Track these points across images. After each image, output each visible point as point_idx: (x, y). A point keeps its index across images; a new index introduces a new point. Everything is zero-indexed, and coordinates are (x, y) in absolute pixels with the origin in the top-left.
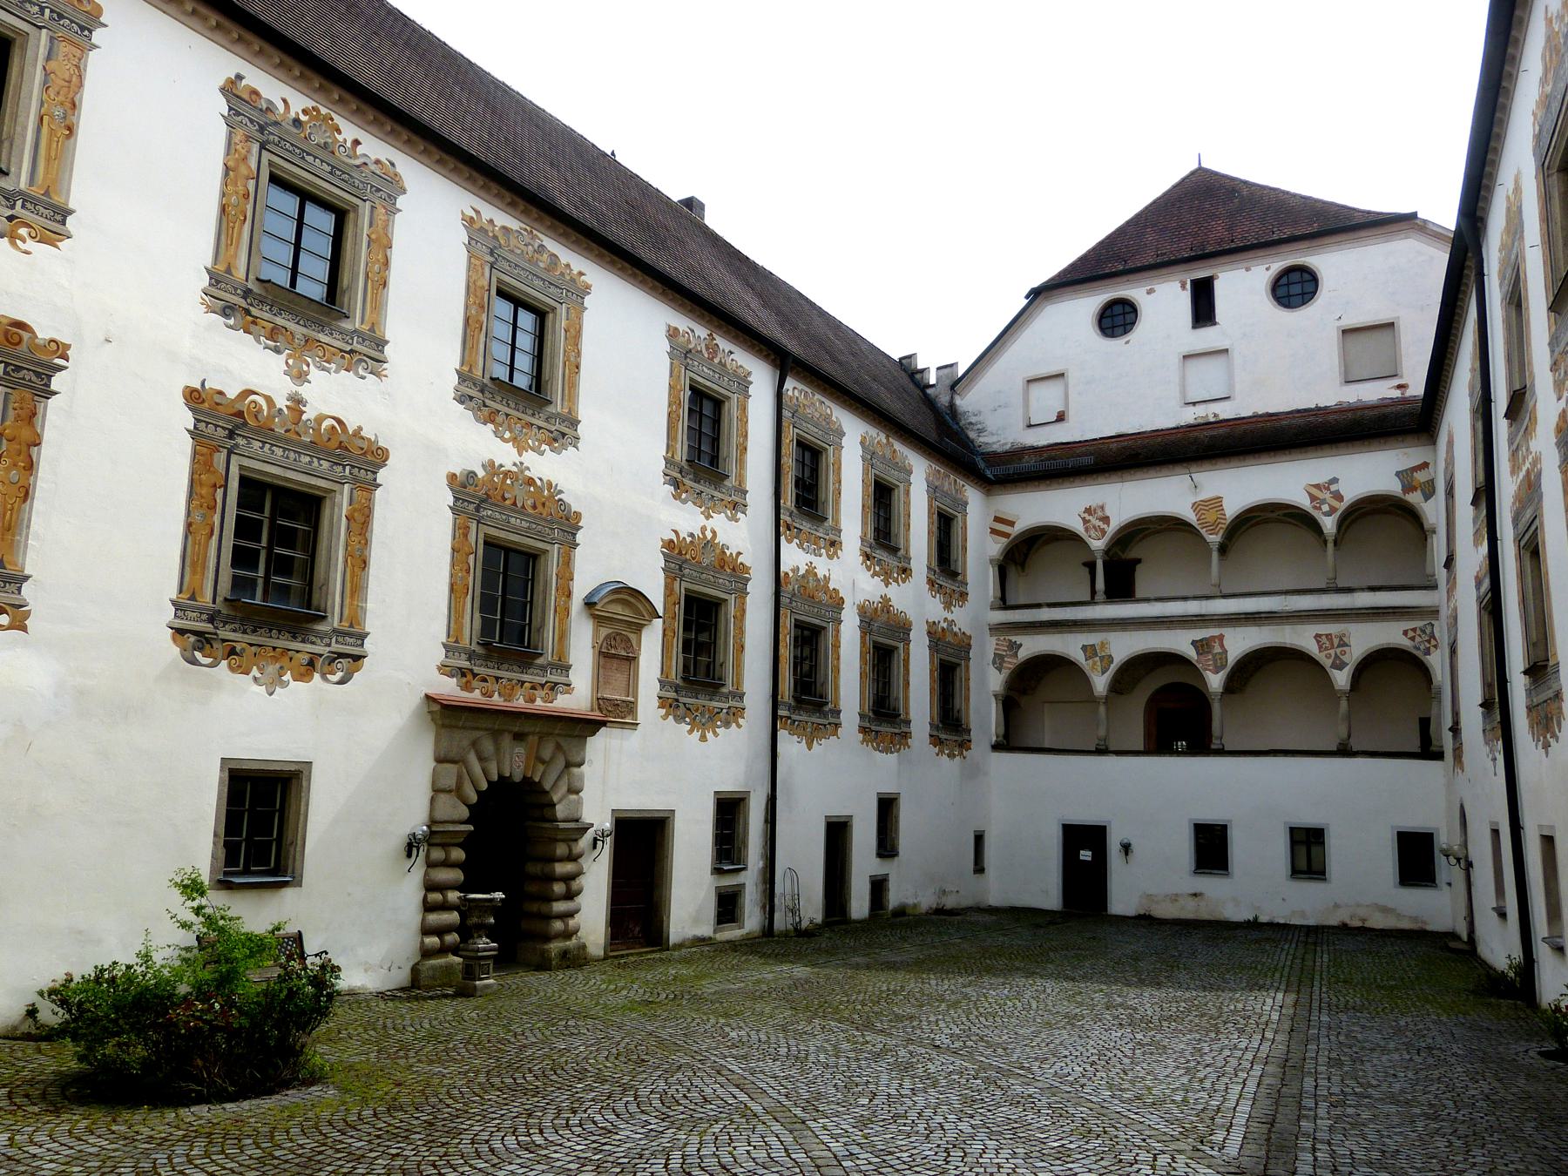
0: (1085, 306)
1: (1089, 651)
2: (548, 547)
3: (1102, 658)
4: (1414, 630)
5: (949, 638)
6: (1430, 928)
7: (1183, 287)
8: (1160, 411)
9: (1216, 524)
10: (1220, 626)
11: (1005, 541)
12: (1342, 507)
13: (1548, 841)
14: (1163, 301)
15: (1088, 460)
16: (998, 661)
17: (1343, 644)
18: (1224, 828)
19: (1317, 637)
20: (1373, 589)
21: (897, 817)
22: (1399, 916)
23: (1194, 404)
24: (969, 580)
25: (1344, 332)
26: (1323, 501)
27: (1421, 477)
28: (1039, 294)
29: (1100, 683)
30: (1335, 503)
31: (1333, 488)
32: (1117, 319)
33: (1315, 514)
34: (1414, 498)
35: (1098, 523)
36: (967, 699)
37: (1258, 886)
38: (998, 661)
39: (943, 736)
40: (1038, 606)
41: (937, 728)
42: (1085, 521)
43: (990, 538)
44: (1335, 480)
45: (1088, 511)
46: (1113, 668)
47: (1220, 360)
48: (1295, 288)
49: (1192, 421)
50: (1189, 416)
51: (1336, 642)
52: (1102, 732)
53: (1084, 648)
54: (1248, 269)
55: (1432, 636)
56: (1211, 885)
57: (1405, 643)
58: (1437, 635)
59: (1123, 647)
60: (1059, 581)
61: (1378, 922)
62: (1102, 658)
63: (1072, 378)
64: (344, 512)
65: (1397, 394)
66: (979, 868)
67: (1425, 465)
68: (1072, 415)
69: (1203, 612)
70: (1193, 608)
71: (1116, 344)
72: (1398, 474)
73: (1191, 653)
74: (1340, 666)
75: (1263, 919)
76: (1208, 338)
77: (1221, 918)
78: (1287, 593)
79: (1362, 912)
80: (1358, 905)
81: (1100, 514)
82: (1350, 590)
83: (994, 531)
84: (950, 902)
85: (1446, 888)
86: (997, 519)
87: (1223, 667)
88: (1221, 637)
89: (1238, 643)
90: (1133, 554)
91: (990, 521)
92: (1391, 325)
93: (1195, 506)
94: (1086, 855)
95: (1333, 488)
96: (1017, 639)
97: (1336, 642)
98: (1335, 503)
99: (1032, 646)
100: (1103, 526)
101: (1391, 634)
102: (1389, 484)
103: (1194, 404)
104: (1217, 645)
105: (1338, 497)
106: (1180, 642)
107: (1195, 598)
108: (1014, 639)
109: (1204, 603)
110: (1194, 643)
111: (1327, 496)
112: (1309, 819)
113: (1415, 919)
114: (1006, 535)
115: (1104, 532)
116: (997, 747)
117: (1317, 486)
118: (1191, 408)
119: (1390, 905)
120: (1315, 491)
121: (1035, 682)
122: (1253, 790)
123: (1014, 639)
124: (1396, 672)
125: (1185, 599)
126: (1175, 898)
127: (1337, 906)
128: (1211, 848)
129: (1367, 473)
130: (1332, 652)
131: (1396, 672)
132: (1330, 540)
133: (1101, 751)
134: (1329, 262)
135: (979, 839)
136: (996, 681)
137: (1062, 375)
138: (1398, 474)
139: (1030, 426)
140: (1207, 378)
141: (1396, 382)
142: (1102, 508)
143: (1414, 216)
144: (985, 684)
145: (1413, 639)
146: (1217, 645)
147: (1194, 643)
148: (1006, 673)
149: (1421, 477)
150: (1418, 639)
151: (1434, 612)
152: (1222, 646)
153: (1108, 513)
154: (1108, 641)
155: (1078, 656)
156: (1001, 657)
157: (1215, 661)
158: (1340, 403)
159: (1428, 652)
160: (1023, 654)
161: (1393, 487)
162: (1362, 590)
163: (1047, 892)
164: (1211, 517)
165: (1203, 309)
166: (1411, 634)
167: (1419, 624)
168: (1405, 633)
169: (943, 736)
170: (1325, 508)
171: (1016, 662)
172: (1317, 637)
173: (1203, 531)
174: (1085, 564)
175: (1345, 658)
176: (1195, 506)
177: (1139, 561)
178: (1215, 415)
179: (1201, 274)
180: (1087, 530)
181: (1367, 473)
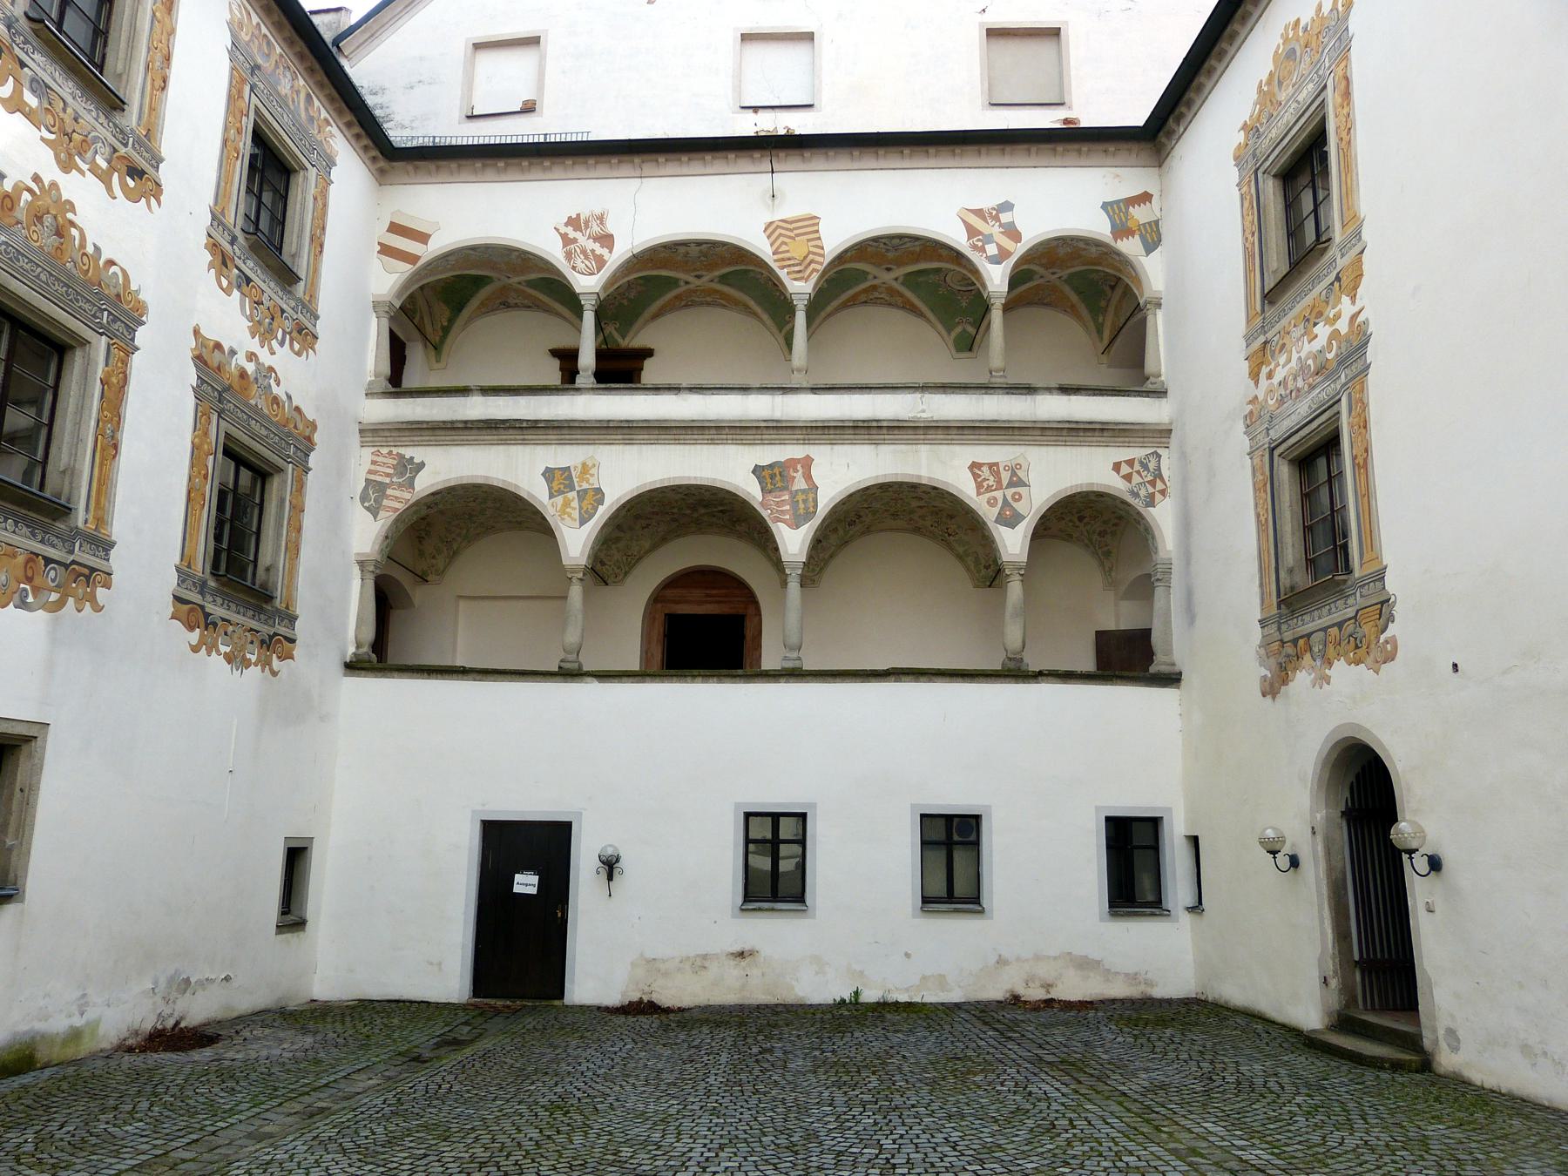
1: (558, 479)
2: (87, 333)
3: (582, 495)
4: (1130, 463)
5: (257, 400)
6: (1159, 992)
9: (806, 262)
11: (406, 269)
12: (1019, 250)
13: (1195, 841)
16: (373, 495)
17: (1017, 482)
18: (568, 825)
19: (975, 466)
20: (1065, 390)
21: (28, 804)
22: (1108, 974)
23: (756, 109)
24: (323, 307)
26: (989, 239)
27: (1140, 214)
29: (576, 542)
30: (1008, 244)
33: (974, 257)
34: (1130, 247)
36: (294, 549)
37: (863, 937)
38: (373, 495)
39: (217, 610)
40: (464, 391)
41: (202, 588)
42: (567, 240)
43: (376, 263)
44: (1007, 207)
45: (574, 222)
46: (603, 513)
47: (798, 52)
51: (1005, 477)
52: (572, 636)
53: (549, 474)
55: (1159, 475)
56: (773, 932)
57: (1114, 484)
58: (1165, 473)
59: (627, 473)
60: (508, 346)
61: (1073, 988)
62: (582, 495)
63: (551, 45)
64: (100, 374)
66: (291, 916)
67: (1145, 198)
69: (777, 415)
72: (1105, 206)
73: (751, 490)
75: (870, 996)
77: (790, 998)
79: (1044, 971)
80: (1038, 958)
81: (596, 229)
82: (1030, 390)
83: (386, 250)
84: (197, 1010)
85: (1186, 919)
86: (395, 228)
88: (807, 462)
89: (840, 473)
90: (637, 341)
91: (381, 233)
93: (771, 229)
94: (526, 883)
96: (416, 453)
97: (1005, 477)
98: (1008, 244)
100: (599, 250)
101: (1092, 469)
103: (756, 109)
104: (799, 476)
105: (1013, 233)
106: (731, 469)
107: (764, 389)
108: (408, 452)
110: (757, 470)
111: (995, 230)
113: (1133, 978)
115: (601, 262)
116: (353, 667)
117: (979, 213)
118: (750, 114)
119: (1095, 955)
121: (445, 545)
122: (852, 743)
123: (408, 452)
124: (1094, 528)
125: (745, 390)
126: (701, 963)
127: (1001, 962)
128: (775, 862)
129: (1062, 203)
130: (999, 494)
133: (569, 673)
135: (296, 856)
136: (365, 534)
139: (471, 117)
142: (601, 219)
144: (334, 540)
145: (1128, 478)
146: (799, 476)
147: (757, 470)
148: (386, 519)
149: (1140, 214)
150: (1136, 479)
151: (1162, 434)
153: (611, 228)
154: (587, 466)
155: (535, 489)
156: (381, 488)
157: (794, 504)
159: (1151, 501)
160: (426, 483)
161: (1097, 226)
162: (1049, 390)
163: (433, 958)
164: (798, 250)
167: (1137, 453)
169: (217, 610)
170: (992, 250)
171: (409, 497)
172: (975, 466)
173: (783, 274)
174: (555, 353)
176: (771, 229)
177: (648, 353)
180: (569, 256)
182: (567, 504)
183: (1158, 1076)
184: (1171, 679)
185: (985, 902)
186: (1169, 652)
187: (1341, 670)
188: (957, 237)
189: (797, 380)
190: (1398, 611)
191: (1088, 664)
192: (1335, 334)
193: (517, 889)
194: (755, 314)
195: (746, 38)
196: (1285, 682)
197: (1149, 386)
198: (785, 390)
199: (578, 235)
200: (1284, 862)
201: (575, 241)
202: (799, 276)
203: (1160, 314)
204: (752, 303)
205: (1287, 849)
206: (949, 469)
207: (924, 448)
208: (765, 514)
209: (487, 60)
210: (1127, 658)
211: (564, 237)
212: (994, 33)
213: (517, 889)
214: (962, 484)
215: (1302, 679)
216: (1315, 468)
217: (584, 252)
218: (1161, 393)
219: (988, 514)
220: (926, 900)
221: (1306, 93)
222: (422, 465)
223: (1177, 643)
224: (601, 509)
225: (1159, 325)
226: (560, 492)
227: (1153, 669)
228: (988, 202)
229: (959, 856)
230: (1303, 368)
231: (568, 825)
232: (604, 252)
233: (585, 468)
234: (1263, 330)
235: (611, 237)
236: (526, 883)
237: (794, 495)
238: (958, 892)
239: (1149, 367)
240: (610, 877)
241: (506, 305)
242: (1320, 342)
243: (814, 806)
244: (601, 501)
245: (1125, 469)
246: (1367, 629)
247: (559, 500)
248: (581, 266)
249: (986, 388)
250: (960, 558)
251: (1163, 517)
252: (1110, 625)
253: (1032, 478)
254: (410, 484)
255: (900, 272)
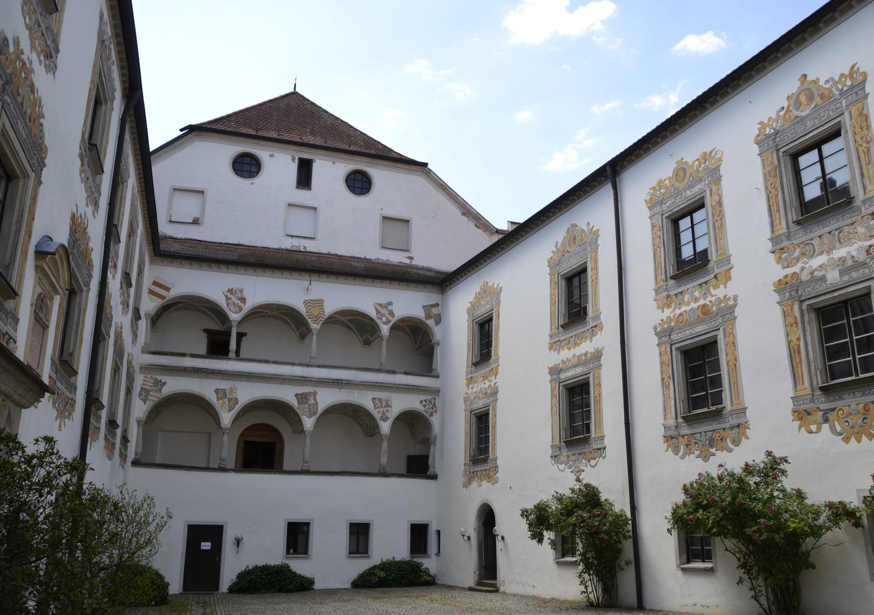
0: (226, 151)
3: (230, 400)
4: (426, 401)
7: (293, 160)
8: (270, 237)
10: (315, 386)
12: (394, 320)
13: (439, 532)
14: (279, 165)
15: (234, 256)
19: (374, 399)
20: (406, 373)
23: (292, 236)
25: (384, 217)
26: (383, 315)
28: (191, 130)
30: (390, 318)
31: (390, 308)
32: (247, 166)
34: (431, 323)
35: (237, 301)
40: (183, 355)
42: (227, 298)
44: (390, 304)
45: (230, 291)
46: (238, 408)
47: (311, 212)
48: (359, 183)
49: (289, 248)
50: (288, 244)
51: (384, 403)
53: (217, 391)
54: (334, 163)
57: (419, 407)
62: (230, 400)
63: (209, 195)
65: (408, 261)
67: (437, 305)
68: (207, 220)
69: (305, 375)
70: (298, 371)
71: (244, 183)
72: (424, 307)
73: (294, 402)
74: (385, 419)
76: (303, 196)
78: (358, 369)
81: (239, 295)
82: (394, 372)
86: (155, 283)
87: (315, 414)
88: (315, 393)
89: (327, 398)
92: (408, 221)
93: (306, 303)
94: (206, 546)
95: (390, 308)
96: (163, 378)
97: (384, 403)
98: (390, 318)
99: (174, 385)
100: (240, 304)
102: (418, 313)
103: (292, 236)
105: (392, 314)
106: (287, 394)
109: (306, 369)
110: (297, 395)
112: (360, 517)
114: (163, 297)
115: (241, 309)
117: (381, 305)
118: (290, 238)
120: (381, 307)
123: (159, 378)
124: (414, 424)
125: (293, 364)
129: (408, 303)
130: (381, 410)
131: (414, 424)
132: (385, 339)
134: (379, 174)
137: (203, 192)
138: (424, 307)
140: (301, 224)
141: (407, 254)
142: (241, 291)
143: (426, 165)
145: (424, 406)
146: (312, 398)
147: (297, 395)
149: (435, 311)
151: (437, 392)
152: (315, 399)
153: (245, 295)
154: (235, 390)
155: (212, 397)
156: (147, 392)
157: (310, 409)
158: (378, 259)
159: (431, 415)
160: (166, 391)
161: (420, 314)
162: (401, 373)
164: (315, 312)
165: (304, 178)
166: (424, 403)
168: (421, 402)
170: (384, 319)
172: (374, 399)
173: (309, 321)
175: (388, 415)
176: (306, 303)
178: (305, 248)
179: (306, 156)
180: (228, 304)
181: (408, 303)
182: (224, 403)
183: (685, 182)
184: (434, 477)
185: (370, 553)
186: (434, 467)
187: (484, 483)
188: (373, 314)
189: (313, 362)
190: (499, 470)
191: (403, 470)
192: (490, 386)
193: (202, 548)
194: (288, 323)
195: (289, 205)
196: (470, 484)
197: (433, 374)
198: (308, 366)
199: (232, 296)
200: (466, 538)
201: (230, 299)
202: (315, 322)
203: (439, 348)
204: (289, 321)
205: (467, 535)
206: (365, 399)
207: (357, 391)
208: (299, 412)
209: (178, 196)
210: (419, 466)
211: (226, 297)
212: (385, 218)
213: (202, 548)
214: (369, 406)
215: (474, 484)
216: (482, 422)
217: (234, 304)
218: (437, 377)
219: (378, 417)
220: (350, 553)
221: (489, 307)
222: (165, 383)
223: (436, 463)
224: (237, 406)
225: (438, 351)
226: (221, 399)
227: (429, 473)
228: (384, 301)
229: (361, 538)
230: (481, 391)
231: (189, 526)
232: (242, 305)
233: (231, 390)
234: (471, 372)
235: (245, 299)
236: (206, 546)
237: (309, 406)
238: (360, 550)
239: (434, 366)
240: (238, 546)
241: (186, 309)
242: (486, 386)
243: (313, 520)
244: (237, 403)
245: (424, 403)
246: (492, 473)
247: (221, 401)
248: (233, 309)
249: (379, 371)
250: (361, 425)
251: (435, 420)
252: (412, 453)
253: (393, 405)
254: (160, 391)
255: (348, 318)
